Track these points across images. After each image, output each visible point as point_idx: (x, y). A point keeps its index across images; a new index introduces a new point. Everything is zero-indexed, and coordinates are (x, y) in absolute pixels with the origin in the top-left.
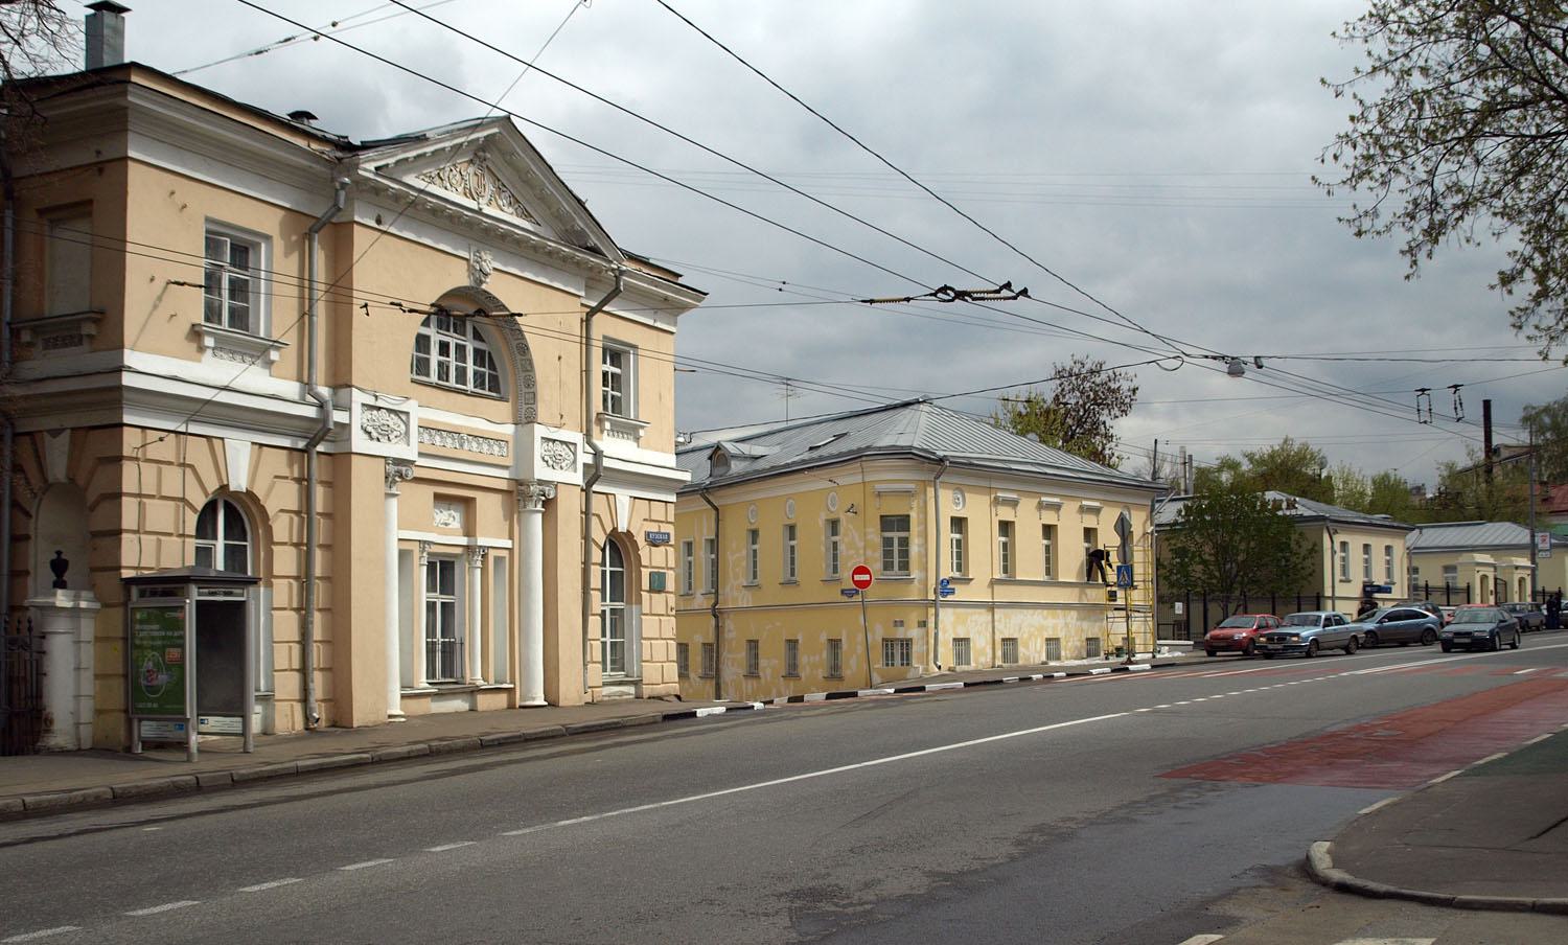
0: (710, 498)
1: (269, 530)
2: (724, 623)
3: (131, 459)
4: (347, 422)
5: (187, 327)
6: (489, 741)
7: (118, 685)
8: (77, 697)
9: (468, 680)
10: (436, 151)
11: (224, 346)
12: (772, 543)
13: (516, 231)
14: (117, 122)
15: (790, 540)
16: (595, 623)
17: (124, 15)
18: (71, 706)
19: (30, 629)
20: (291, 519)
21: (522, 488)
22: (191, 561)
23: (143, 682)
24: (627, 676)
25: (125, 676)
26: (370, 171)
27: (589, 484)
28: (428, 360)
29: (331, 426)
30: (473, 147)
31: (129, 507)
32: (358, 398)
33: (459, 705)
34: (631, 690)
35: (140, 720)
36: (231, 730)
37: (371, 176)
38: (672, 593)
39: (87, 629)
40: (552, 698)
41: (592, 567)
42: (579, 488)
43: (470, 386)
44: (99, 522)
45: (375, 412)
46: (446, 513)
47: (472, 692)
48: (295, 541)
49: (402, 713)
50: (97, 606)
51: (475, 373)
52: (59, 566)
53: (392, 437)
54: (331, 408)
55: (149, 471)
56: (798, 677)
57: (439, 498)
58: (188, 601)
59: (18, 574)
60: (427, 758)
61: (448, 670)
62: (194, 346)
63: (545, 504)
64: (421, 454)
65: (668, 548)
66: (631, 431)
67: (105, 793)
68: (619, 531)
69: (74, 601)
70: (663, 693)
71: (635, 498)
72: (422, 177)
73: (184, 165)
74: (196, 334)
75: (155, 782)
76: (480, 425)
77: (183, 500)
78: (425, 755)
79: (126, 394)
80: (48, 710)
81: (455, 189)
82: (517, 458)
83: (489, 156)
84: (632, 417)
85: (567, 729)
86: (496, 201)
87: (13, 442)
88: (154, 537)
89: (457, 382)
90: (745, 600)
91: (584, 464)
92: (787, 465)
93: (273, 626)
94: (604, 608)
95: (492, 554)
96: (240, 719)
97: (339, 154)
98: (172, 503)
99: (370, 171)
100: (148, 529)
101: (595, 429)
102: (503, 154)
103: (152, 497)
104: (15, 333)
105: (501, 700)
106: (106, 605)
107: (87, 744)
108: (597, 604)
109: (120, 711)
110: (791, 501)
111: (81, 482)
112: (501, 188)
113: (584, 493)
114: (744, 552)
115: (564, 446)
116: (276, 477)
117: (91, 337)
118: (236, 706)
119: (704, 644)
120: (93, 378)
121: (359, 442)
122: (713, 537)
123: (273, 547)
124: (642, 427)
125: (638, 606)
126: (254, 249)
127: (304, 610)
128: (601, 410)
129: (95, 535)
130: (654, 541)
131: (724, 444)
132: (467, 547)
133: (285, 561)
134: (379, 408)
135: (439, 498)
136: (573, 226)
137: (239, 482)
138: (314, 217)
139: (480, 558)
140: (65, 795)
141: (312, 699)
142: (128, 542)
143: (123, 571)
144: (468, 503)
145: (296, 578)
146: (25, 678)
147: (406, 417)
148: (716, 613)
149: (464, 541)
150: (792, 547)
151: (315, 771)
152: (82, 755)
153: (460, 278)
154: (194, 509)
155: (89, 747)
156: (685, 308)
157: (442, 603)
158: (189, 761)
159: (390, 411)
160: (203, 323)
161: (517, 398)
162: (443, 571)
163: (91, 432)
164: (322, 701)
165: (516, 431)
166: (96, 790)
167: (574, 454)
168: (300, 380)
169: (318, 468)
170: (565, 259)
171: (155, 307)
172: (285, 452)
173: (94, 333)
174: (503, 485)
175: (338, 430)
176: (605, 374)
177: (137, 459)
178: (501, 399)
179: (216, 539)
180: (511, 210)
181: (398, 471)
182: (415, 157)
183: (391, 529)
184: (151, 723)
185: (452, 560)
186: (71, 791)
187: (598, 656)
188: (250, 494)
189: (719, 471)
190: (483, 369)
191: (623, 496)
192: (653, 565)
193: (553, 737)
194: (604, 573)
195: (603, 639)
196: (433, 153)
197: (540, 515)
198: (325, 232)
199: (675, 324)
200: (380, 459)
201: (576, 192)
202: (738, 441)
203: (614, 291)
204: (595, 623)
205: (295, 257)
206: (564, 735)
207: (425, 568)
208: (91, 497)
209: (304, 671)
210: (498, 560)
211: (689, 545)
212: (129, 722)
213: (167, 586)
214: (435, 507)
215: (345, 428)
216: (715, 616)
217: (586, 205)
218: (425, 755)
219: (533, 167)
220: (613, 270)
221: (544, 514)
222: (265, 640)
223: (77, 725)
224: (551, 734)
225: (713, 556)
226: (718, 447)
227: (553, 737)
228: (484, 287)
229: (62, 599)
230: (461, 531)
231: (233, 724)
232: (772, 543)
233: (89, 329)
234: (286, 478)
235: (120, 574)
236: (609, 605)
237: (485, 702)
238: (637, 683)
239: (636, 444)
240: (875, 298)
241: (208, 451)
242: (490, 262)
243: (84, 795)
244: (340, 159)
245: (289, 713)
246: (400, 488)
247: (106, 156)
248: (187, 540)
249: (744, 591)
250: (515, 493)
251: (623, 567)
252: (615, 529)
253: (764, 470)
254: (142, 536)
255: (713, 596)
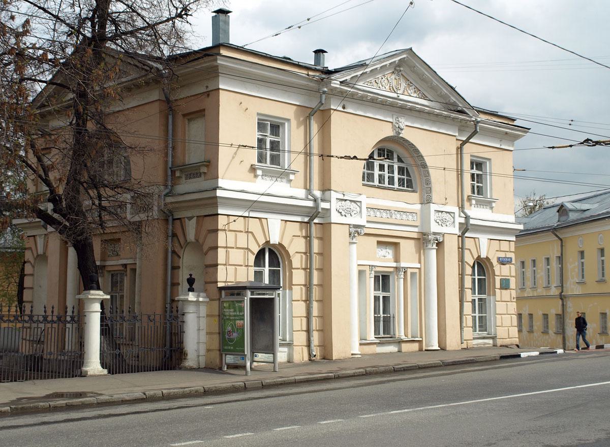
0: (558, 234)
1: (290, 262)
2: (566, 303)
3: (222, 230)
4: (329, 208)
5: (249, 166)
6: (398, 368)
7: (216, 338)
8: (198, 343)
9: (397, 336)
10: (353, 77)
11: (266, 173)
12: (592, 258)
13: (417, 106)
14: (214, 73)
15: (582, 259)
16: (468, 307)
17: (228, 14)
18: (195, 347)
19: (177, 311)
20: (302, 256)
21: (425, 237)
22: (252, 278)
23: (227, 337)
24: (488, 334)
25: (219, 333)
26: (337, 84)
27: (463, 233)
28: (373, 174)
29: (320, 210)
30: (393, 65)
31: (221, 253)
32: (334, 196)
33: (392, 349)
34: (491, 341)
35: (226, 355)
36: (268, 360)
37: (338, 86)
38: (514, 289)
39: (203, 310)
40: (443, 346)
41: (466, 277)
42: (457, 236)
43: (396, 186)
44: (209, 261)
45: (343, 202)
46: (384, 251)
47: (399, 342)
48: (303, 267)
49: (360, 353)
50: (207, 300)
51: (399, 179)
52: (191, 281)
53: (352, 214)
54: (320, 201)
55: (231, 235)
56: (607, 334)
57: (379, 243)
58: (246, 298)
59: (175, 285)
60: (364, 376)
61: (387, 330)
62: (252, 175)
63: (438, 245)
64: (368, 222)
65: (511, 265)
66: (488, 204)
67: (200, 389)
68: (482, 257)
69: (197, 297)
70: (509, 343)
71: (491, 239)
72: (367, 83)
73: (246, 89)
74: (253, 169)
75: (224, 385)
76: (401, 206)
77: (247, 249)
78: (363, 375)
79: (219, 200)
80: (185, 349)
81: (385, 86)
82: (422, 223)
83: (402, 69)
84: (489, 197)
85: (443, 363)
86: (407, 90)
87: (173, 224)
88: (234, 267)
89: (389, 184)
90: (578, 290)
91: (460, 223)
92: (599, 215)
93: (291, 310)
94: (474, 298)
95: (409, 271)
96: (272, 355)
97: (324, 76)
98: (242, 250)
99: (337, 84)
100: (230, 263)
101: (466, 204)
102: (410, 67)
103: (233, 248)
104: (173, 172)
105: (415, 346)
106: (211, 300)
107: (202, 365)
108: (469, 295)
109: (217, 350)
110: (601, 235)
111: (201, 241)
112: (410, 84)
113: (460, 238)
114: (577, 264)
115: (448, 214)
116: (294, 236)
117: (205, 173)
118: (270, 349)
119: (557, 315)
120: (205, 193)
121: (335, 217)
122: (560, 255)
123: (292, 270)
124: (494, 202)
125: (494, 297)
126: (282, 126)
127: (308, 301)
128: (470, 194)
129: (207, 266)
130: (502, 262)
131: (565, 203)
132: (396, 268)
133: (299, 277)
134: (346, 200)
135: (379, 243)
136: (449, 100)
137: (275, 240)
138: (311, 108)
139: (403, 273)
140: (182, 390)
141: (312, 345)
142: (221, 270)
143: (218, 283)
144: (396, 245)
145: (305, 285)
146: (178, 333)
147: (359, 203)
148: (562, 297)
149: (394, 265)
150: (603, 261)
151: (281, 384)
152: (200, 371)
153: (388, 132)
154: (253, 253)
155: (204, 367)
156: (517, 137)
157: (383, 297)
158: (246, 375)
159: (351, 201)
160: (257, 164)
161: (422, 190)
162: (383, 280)
163: (205, 218)
164: (318, 346)
165: (422, 206)
166: (196, 388)
167: (454, 218)
168: (305, 188)
169: (314, 230)
170: (446, 117)
171: (233, 158)
172: (298, 223)
173: (206, 171)
174: (415, 236)
175: (325, 212)
176: (473, 175)
177: (225, 230)
178: (413, 191)
179: (265, 267)
180: (415, 95)
181: (356, 231)
182: (361, 75)
183: (352, 261)
184: (230, 356)
185: (389, 274)
186: (185, 388)
187: (470, 323)
188: (280, 244)
189: (563, 218)
190: (403, 177)
191: (484, 239)
192: (502, 275)
193: (435, 367)
194: (474, 280)
195: (474, 315)
196: (381, 67)
197: (435, 250)
198: (317, 114)
199: (513, 146)
200: (346, 226)
201: (449, 83)
202: (573, 202)
203: (474, 132)
204: (468, 307)
205: (302, 128)
206: (441, 366)
207: (373, 279)
208: (205, 248)
209: (308, 331)
210: (413, 274)
211: (523, 263)
212: (221, 355)
213: (236, 291)
214: (378, 248)
215: (328, 211)
216: (561, 299)
217: (456, 89)
218: (363, 375)
219: (426, 73)
220: (473, 121)
221: (437, 250)
222: (289, 315)
223: (198, 356)
224: (433, 365)
225: (560, 266)
226: (562, 205)
227: (435, 367)
228: (401, 135)
229: (192, 297)
230: (393, 260)
231: (269, 357)
232: (592, 258)
233: (204, 170)
234: (299, 236)
235: (217, 285)
236: (477, 297)
237: (406, 347)
238: (494, 338)
239: (491, 211)
240: (555, 146)
241: (260, 225)
242: (404, 122)
243: (190, 390)
244: (322, 80)
245: (301, 353)
246: (358, 239)
247: (210, 88)
248: (249, 268)
249: (577, 285)
250: (421, 240)
251: (485, 276)
252: (479, 256)
253: (587, 218)
254: (228, 267)
255: (560, 288)
